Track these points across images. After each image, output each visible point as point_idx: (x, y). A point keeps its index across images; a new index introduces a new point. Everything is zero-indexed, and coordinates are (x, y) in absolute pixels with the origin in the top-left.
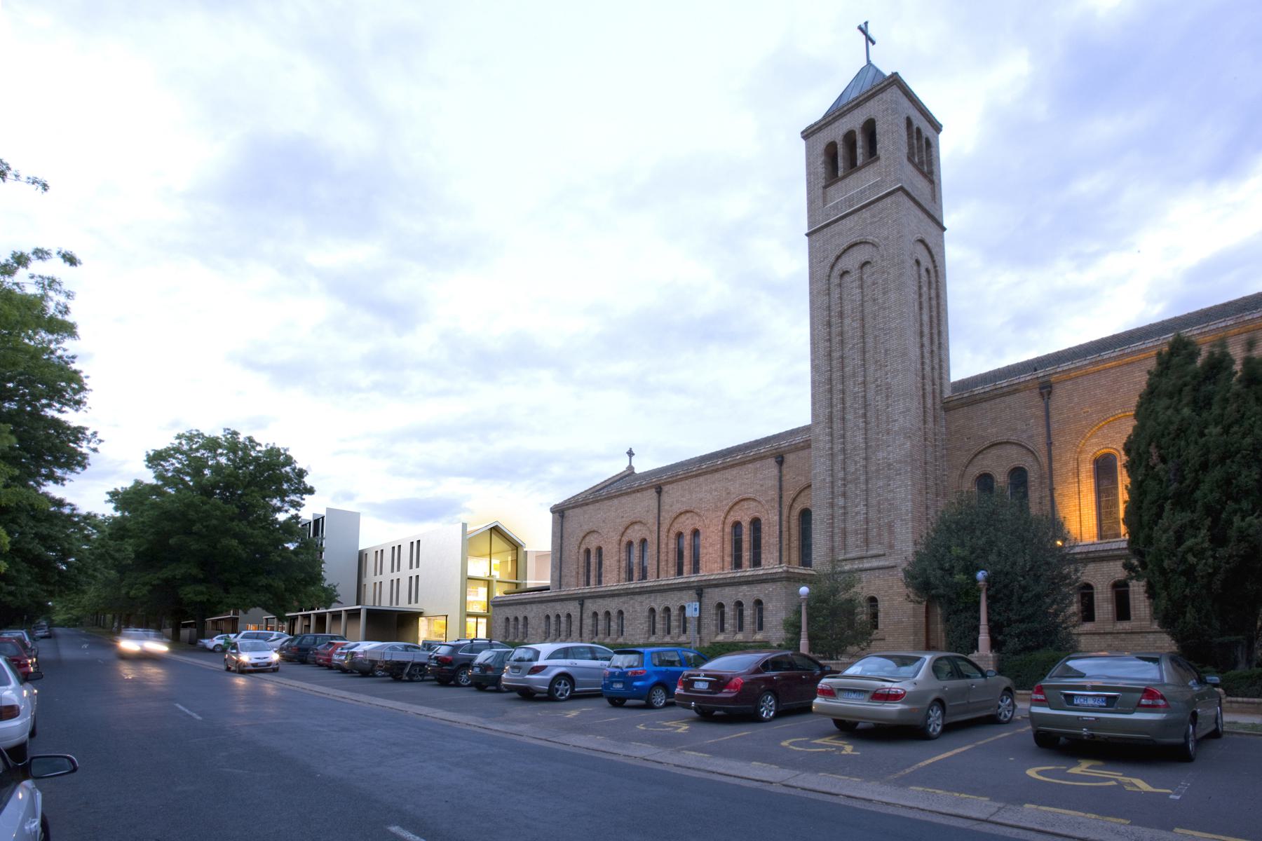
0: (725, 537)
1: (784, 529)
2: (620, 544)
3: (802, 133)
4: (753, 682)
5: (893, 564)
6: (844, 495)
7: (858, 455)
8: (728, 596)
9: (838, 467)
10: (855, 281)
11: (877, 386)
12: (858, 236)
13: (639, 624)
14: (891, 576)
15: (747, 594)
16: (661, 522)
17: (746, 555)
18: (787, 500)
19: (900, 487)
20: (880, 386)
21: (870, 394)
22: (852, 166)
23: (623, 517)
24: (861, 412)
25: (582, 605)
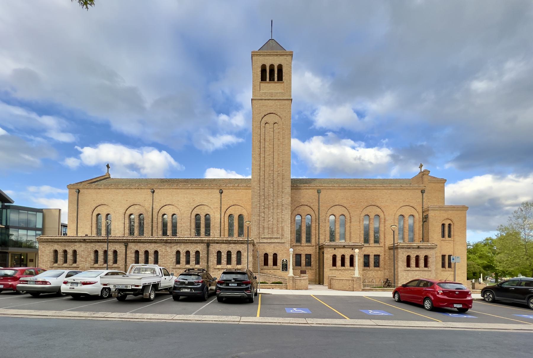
1: (222, 221)
4: (400, 288)
5: (284, 242)
6: (264, 212)
7: (270, 198)
8: (224, 249)
9: (262, 201)
10: (271, 128)
11: (278, 173)
12: (274, 111)
13: (170, 258)
14: (283, 246)
15: (234, 249)
17: (203, 230)
18: (223, 210)
19: (287, 214)
20: (280, 174)
21: (275, 176)
24: (272, 182)
25: (126, 247)
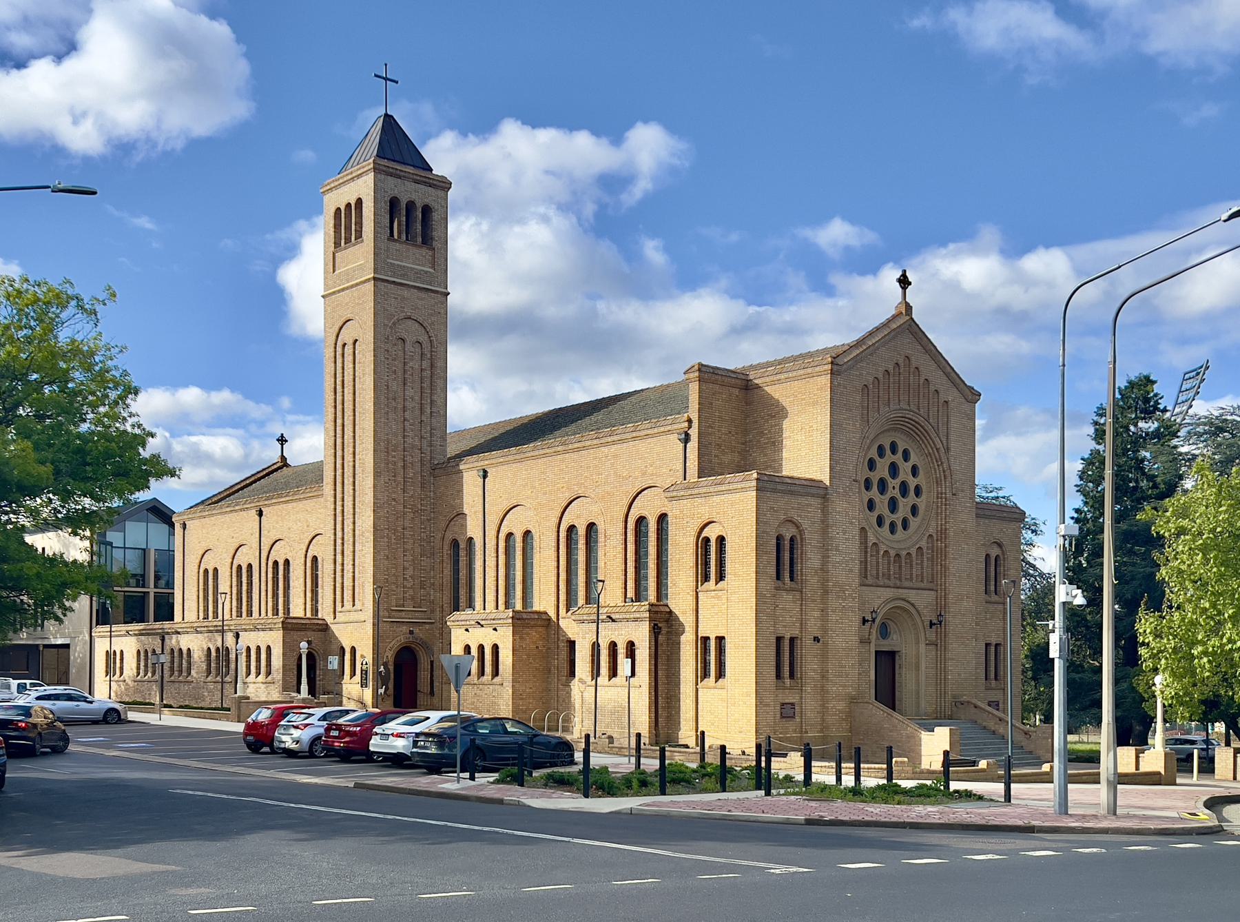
25: (163, 640)
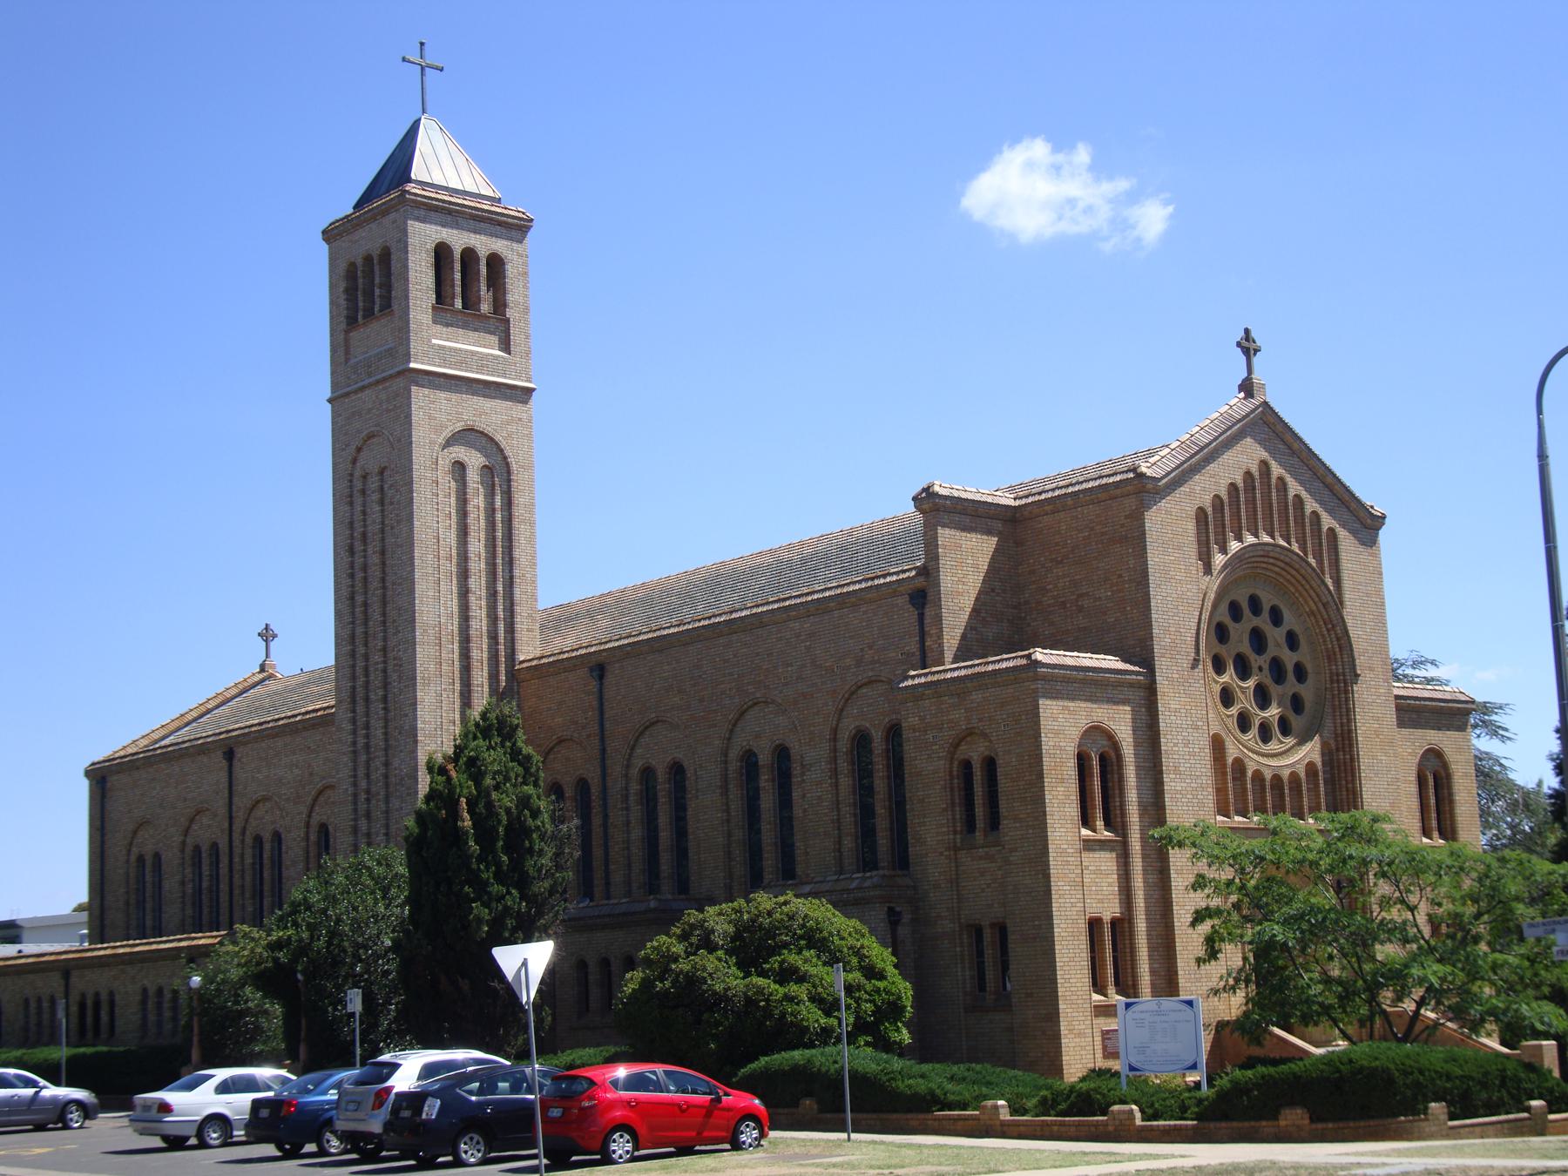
0: (311, 849)
2: (183, 851)
3: (324, 232)
16: (234, 815)
22: (369, 314)
23: (185, 800)
